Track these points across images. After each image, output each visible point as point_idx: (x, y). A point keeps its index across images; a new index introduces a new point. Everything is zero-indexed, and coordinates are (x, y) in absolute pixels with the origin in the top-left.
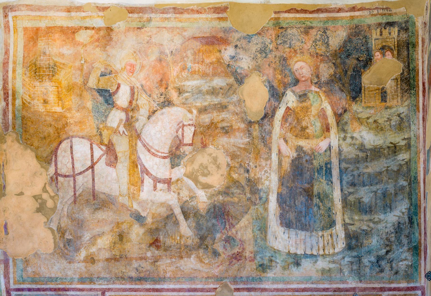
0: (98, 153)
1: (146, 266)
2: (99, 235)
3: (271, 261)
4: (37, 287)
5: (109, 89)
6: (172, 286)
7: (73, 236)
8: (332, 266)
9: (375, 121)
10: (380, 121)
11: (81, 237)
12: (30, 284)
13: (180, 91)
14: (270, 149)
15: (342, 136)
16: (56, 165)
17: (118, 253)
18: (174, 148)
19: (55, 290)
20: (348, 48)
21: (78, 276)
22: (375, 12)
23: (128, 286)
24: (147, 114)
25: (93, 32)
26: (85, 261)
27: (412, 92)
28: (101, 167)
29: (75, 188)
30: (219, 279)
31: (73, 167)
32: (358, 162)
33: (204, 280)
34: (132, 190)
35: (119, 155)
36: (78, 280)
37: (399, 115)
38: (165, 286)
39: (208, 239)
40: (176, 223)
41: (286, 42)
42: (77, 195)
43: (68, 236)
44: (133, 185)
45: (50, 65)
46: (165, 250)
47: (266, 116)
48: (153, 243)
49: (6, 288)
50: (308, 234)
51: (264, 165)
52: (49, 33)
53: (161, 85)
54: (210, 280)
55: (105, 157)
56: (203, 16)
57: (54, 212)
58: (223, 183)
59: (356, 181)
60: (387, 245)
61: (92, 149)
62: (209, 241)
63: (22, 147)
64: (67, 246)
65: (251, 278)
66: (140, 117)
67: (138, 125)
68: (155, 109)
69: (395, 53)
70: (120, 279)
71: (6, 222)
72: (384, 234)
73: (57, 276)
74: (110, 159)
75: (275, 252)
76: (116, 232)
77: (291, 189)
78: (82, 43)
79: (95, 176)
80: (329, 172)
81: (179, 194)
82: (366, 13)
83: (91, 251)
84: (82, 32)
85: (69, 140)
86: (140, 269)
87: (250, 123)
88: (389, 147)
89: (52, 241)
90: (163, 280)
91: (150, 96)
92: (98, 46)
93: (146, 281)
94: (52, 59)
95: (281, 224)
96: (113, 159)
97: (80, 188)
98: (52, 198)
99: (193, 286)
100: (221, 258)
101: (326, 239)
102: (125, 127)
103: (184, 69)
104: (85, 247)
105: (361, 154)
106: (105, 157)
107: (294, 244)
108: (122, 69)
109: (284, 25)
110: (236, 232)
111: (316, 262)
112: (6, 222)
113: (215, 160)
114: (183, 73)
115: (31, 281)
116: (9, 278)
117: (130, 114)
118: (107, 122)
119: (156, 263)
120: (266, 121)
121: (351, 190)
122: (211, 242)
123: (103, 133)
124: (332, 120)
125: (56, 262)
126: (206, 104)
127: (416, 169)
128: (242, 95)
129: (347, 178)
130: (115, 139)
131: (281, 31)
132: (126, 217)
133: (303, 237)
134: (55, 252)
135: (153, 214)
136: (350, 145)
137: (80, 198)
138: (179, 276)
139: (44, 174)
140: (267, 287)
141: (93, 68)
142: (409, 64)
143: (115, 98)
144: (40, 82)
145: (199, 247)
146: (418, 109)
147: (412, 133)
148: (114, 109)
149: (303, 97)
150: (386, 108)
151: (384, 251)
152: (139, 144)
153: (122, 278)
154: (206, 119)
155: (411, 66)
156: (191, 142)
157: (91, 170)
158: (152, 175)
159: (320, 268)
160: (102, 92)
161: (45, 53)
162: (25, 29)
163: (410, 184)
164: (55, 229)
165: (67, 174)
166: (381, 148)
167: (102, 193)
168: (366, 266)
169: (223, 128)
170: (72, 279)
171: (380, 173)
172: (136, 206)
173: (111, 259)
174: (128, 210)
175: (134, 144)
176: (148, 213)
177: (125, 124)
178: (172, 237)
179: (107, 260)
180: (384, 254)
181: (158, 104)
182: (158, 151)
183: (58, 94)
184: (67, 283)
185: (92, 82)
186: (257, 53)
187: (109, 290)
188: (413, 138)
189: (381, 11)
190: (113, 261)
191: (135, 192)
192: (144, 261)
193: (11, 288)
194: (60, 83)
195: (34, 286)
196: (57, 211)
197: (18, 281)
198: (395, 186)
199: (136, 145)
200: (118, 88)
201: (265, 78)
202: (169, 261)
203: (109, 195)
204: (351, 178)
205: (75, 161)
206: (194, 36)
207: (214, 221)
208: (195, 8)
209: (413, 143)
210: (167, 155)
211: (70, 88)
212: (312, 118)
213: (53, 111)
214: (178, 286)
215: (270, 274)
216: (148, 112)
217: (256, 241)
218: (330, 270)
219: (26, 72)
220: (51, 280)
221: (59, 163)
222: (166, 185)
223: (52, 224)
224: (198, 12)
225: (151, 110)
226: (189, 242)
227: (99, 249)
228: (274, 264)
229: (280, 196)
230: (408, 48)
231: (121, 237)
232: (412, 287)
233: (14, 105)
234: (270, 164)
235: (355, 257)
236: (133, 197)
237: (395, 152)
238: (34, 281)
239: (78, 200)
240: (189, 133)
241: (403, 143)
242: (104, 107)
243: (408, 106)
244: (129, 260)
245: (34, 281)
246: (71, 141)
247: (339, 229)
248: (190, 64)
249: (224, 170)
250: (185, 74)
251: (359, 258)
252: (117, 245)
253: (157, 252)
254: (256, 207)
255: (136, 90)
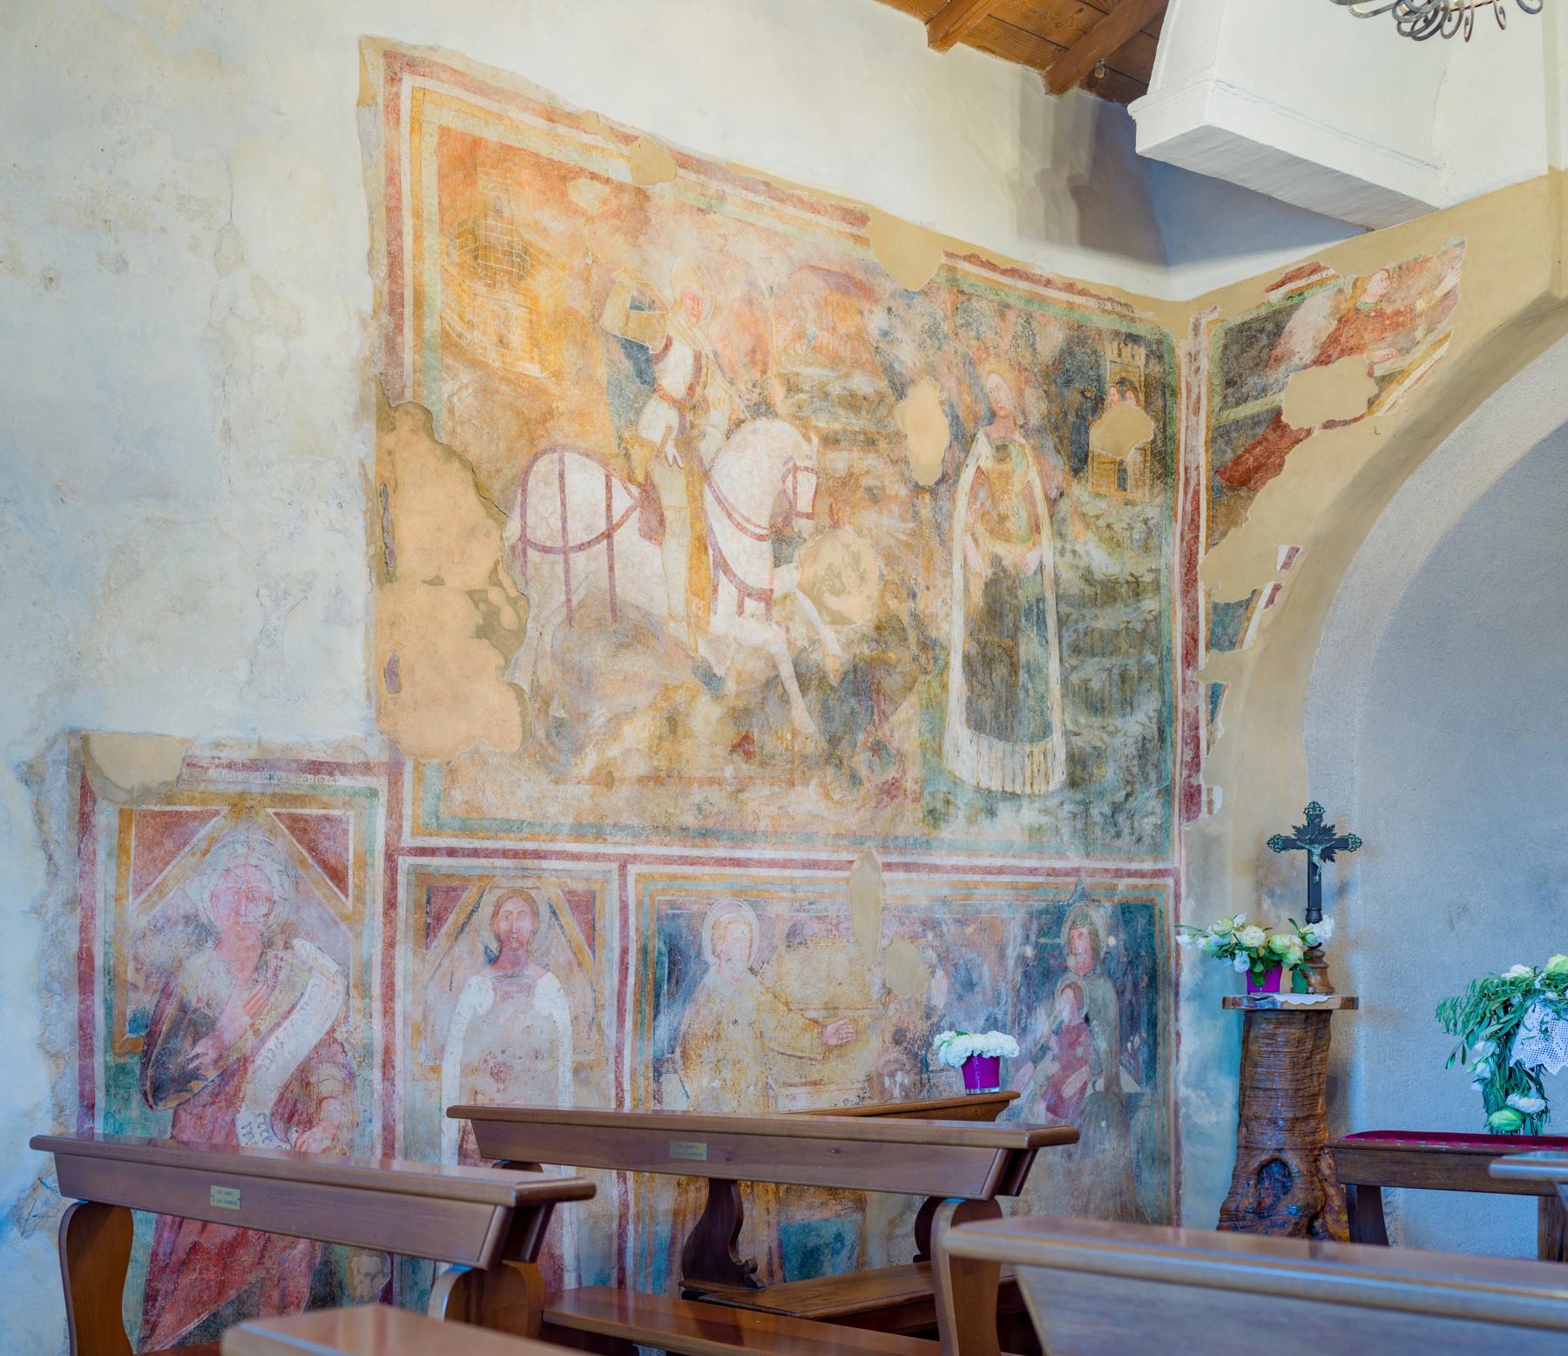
0: (622, 502)
1: (718, 799)
2: (626, 713)
3: (948, 802)
4: (471, 846)
5: (647, 344)
6: (769, 854)
7: (568, 712)
8: (1044, 820)
9: (1109, 526)
10: (1116, 527)
11: (586, 716)
12: (456, 836)
13: (792, 388)
14: (950, 554)
15: (1059, 545)
16: (523, 515)
17: (664, 765)
18: (780, 519)
19: (516, 854)
20: (1068, 366)
21: (571, 820)
22: (1108, 306)
23: (677, 851)
24: (724, 426)
25: (607, 189)
26: (593, 780)
27: (1169, 481)
28: (628, 536)
29: (567, 583)
30: (858, 841)
31: (564, 528)
32: (1084, 605)
33: (830, 841)
34: (694, 608)
35: (669, 515)
36: (571, 829)
37: (1146, 522)
38: (755, 854)
39: (844, 743)
40: (785, 699)
41: (970, 324)
42: (574, 603)
43: (557, 711)
44: (696, 594)
45: (512, 247)
46: (763, 764)
47: (943, 479)
48: (739, 745)
49: (387, 845)
50: (1008, 747)
51: (941, 586)
52: (506, 160)
53: (754, 363)
54: (841, 843)
55: (636, 514)
56: (823, 220)
57: (521, 643)
58: (869, 616)
59: (1081, 644)
60: (1128, 782)
61: (609, 488)
62: (844, 748)
63: (438, 452)
64: (555, 738)
65: (911, 841)
66: (709, 430)
67: (706, 447)
68: (742, 417)
69: (1142, 397)
70: (660, 830)
71: (394, 655)
72: (1123, 759)
73: (522, 817)
74: (648, 521)
75: (955, 783)
76: (662, 708)
77: (983, 646)
78: (584, 213)
79: (616, 560)
80: (1041, 622)
81: (788, 630)
82: (1092, 303)
83: (610, 754)
84: (583, 182)
85: (556, 455)
86: (706, 806)
87: (918, 490)
88: (1128, 582)
89: (517, 720)
90: (745, 837)
91: (732, 383)
92: (618, 229)
93: (718, 840)
94: (518, 233)
95: (968, 720)
96: (654, 523)
97: (580, 585)
98: (513, 602)
99: (813, 856)
100: (863, 791)
101: (1036, 760)
102: (676, 446)
103: (800, 335)
104: (597, 743)
105: (1088, 590)
106: (636, 514)
107: (986, 769)
108: (675, 302)
109: (965, 288)
110: (892, 731)
111: (1018, 810)
112: (394, 655)
113: (857, 559)
114: (798, 346)
115: (461, 829)
116: (401, 817)
117: (689, 417)
118: (641, 426)
119: (740, 795)
120: (943, 489)
121: (1074, 662)
122: (849, 751)
123: (632, 452)
124: (1042, 509)
125: (523, 778)
126: (837, 426)
127: (1170, 633)
128: (903, 423)
129: (1069, 636)
130: (660, 475)
131: (961, 298)
132: (687, 676)
133: (1000, 754)
134: (525, 750)
135: (740, 673)
136: (1071, 566)
137: (582, 611)
138: (785, 829)
139: (495, 534)
140: (939, 862)
141: (613, 282)
142: (1165, 424)
143: (659, 368)
144: (489, 285)
145: (827, 762)
146: (1176, 515)
147: (1163, 560)
148: (655, 396)
149: (1002, 450)
150: (1126, 504)
151: (1123, 793)
152: (709, 497)
153: (664, 828)
154: (840, 461)
155: (1169, 431)
156: (810, 511)
157: (605, 542)
158: (735, 576)
159: (1025, 823)
160: (634, 349)
161: (498, 212)
162: (445, 132)
163: (1160, 662)
164: (526, 687)
165: (549, 544)
166: (1116, 582)
167: (633, 606)
168: (1095, 824)
169: (869, 489)
170: (556, 825)
171: (1117, 633)
172: (703, 650)
173: (649, 778)
174: (688, 656)
175: (697, 494)
176: (728, 669)
177: (677, 440)
178: (776, 732)
179: (642, 780)
180: (1122, 799)
181: (747, 407)
182: (747, 520)
183: (532, 328)
184: (543, 837)
185: (613, 317)
186: (925, 336)
187: (636, 858)
188: (1164, 572)
189: (1118, 308)
190: (652, 783)
191: (700, 613)
192: (716, 787)
193: (403, 845)
194: (535, 299)
195: (465, 843)
196: (527, 640)
197: (427, 826)
198: (1139, 662)
199: (701, 495)
200: (667, 347)
201: (945, 395)
202: (766, 792)
203: (647, 612)
204: (1074, 637)
205: (569, 514)
206: (811, 263)
207: (853, 702)
208: (806, 196)
209: (1163, 580)
210: (764, 532)
211: (563, 319)
212: (1015, 500)
213: (520, 370)
214: (781, 855)
215: (945, 833)
216: (726, 421)
217: (925, 755)
218: (1040, 829)
219: (451, 249)
220: (509, 827)
221: (529, 512)
222: (763, 604)
223: (517, 675)
224: (814, 209)
225: (734, 417)
226: (810, 749)
227: (627, 750)
228: (952, 810)
229: (967, 660)
230: (1164, 393)
231: (673, 723)
232: (1160, 870)
233: (419, 331)
234: (951, 586)
235: (1078, 803)
236: (697, 624)
237: (1138, 595)
238: (467, 830)
239: (577, 616)
240: (806, 486)
241: (1148, 578)
242: (633, 388)
243: (1161, 506)
244: (685, 781)
245: (467, 830)
246: (561, 460)
247: (1057, 743)
248: (814, 329)
249: (873, 588)
250: (801, 348)
251: (1086, 805)
252: (666, 744)
253: (744, 767)
254: (928, 678)
255: (703, 362)
